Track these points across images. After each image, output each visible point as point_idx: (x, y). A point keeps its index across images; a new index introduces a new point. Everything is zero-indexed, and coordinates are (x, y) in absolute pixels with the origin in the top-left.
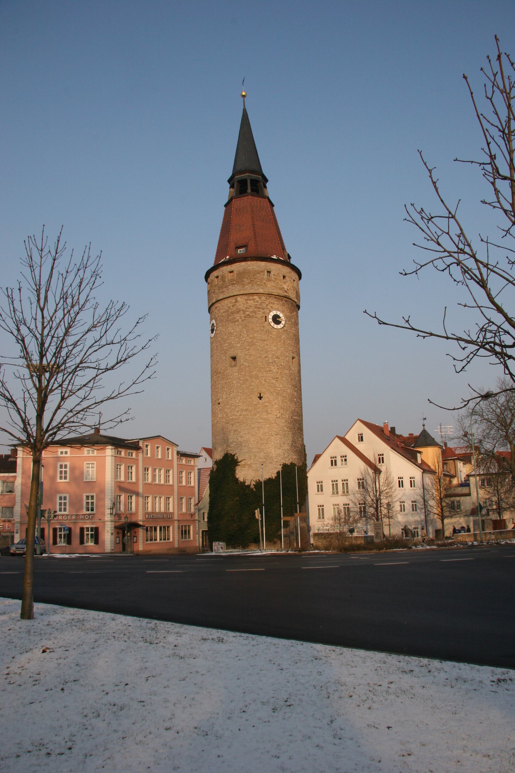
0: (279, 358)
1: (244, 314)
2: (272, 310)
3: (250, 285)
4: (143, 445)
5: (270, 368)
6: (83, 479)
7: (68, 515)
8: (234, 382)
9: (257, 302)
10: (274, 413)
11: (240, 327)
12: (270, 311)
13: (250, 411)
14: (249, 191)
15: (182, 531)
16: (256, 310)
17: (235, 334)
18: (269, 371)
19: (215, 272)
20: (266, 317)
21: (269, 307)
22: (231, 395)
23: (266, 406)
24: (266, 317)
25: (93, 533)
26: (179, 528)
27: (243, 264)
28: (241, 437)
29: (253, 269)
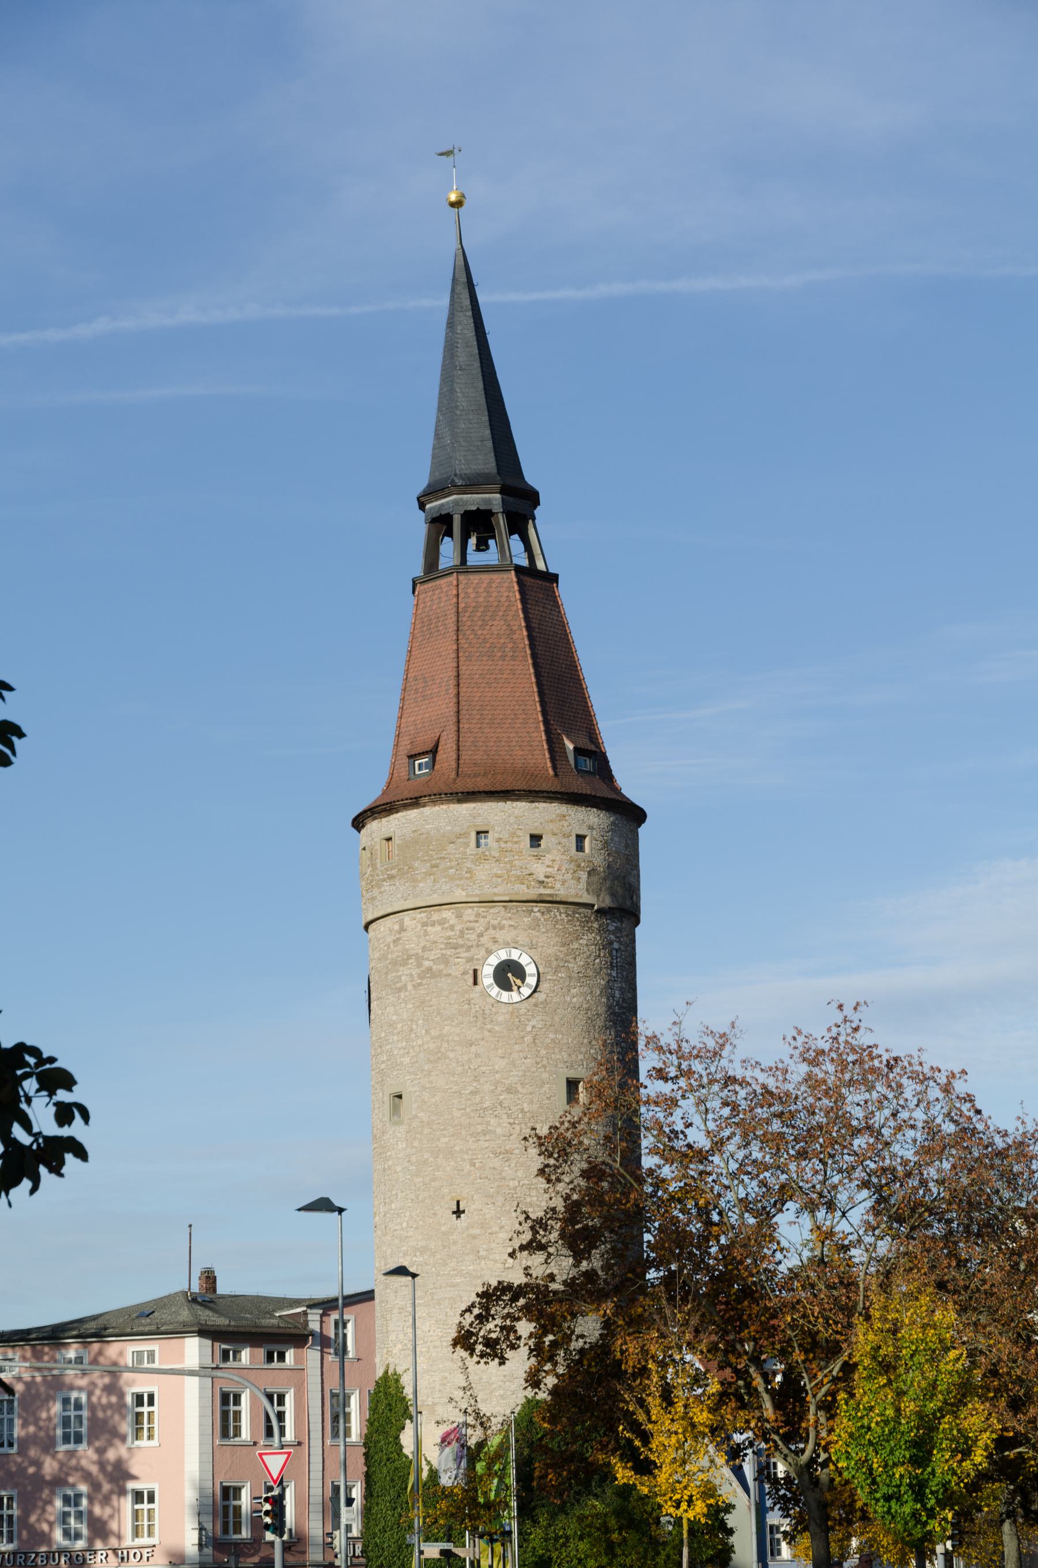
0: (517, 1092)
2: (494, 948)
5: (488, 1123)
11: (410, 1006)
12: (489, 952)
16: (449, 952)
18: (485, 1133)
20: (475, 971)
21: (484, 940)
22: (393, 1206)
23: (475, 1237)
24: (475, 971)
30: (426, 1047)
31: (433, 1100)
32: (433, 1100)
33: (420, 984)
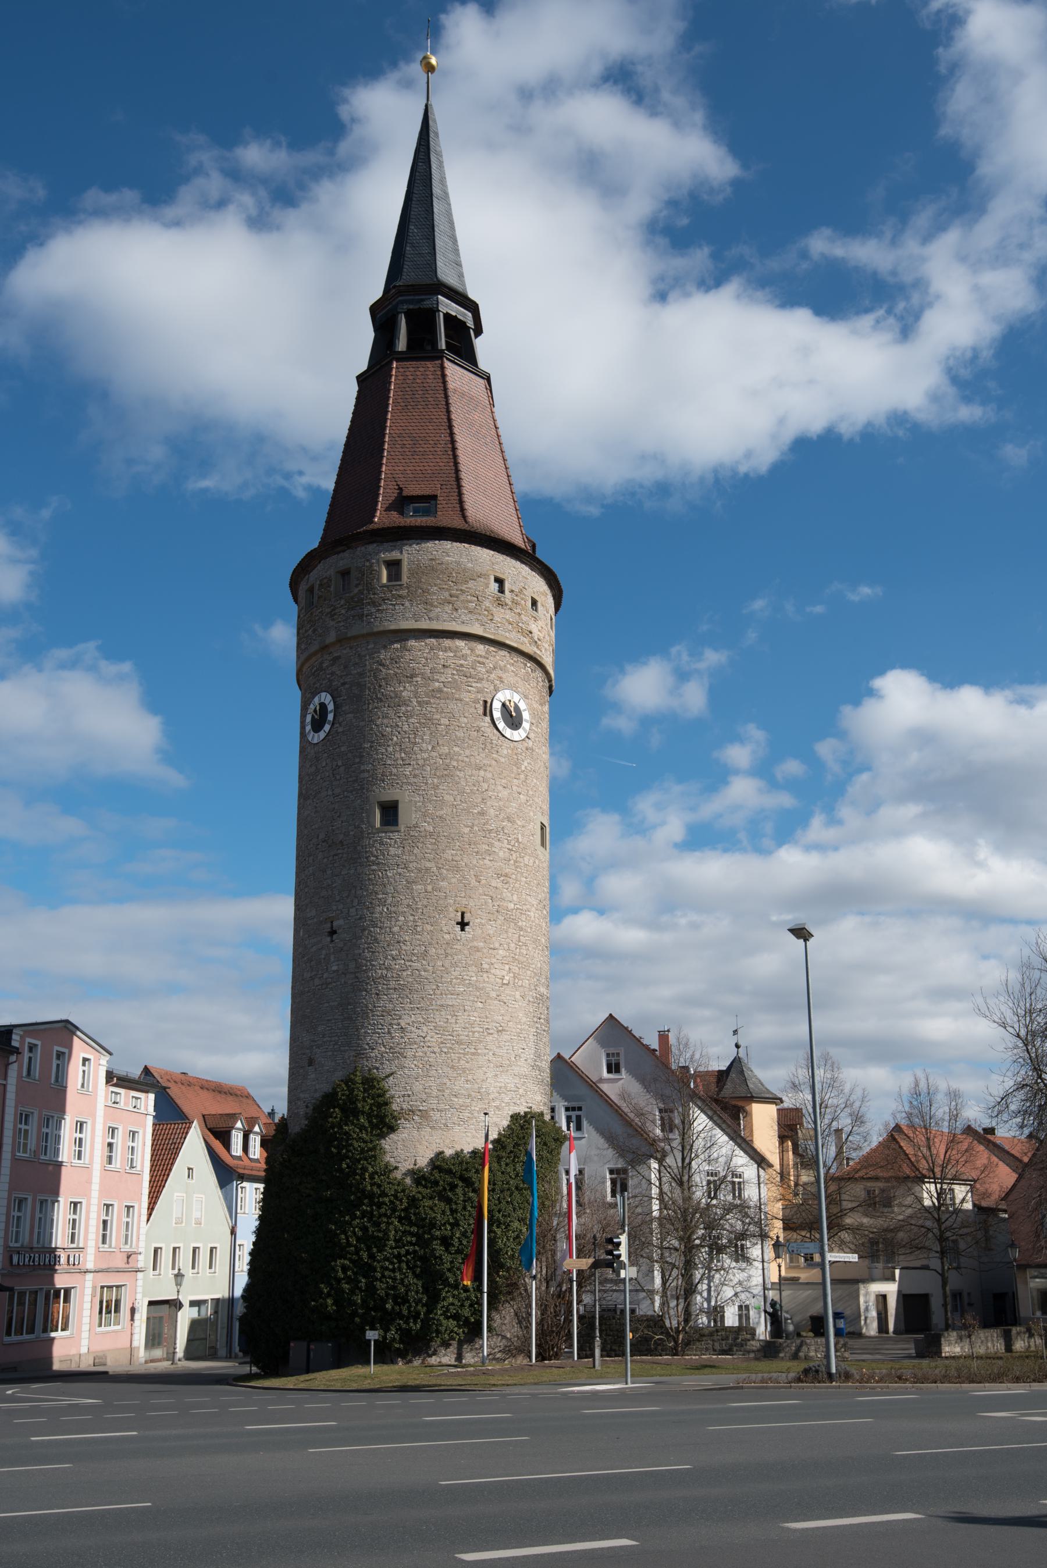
4: (22, 1041)
10: (498, 972)
15: (101, 1302)
19: (527, 569)
21: (493, 676)
26: (93, 1296)
29: (458, 563)
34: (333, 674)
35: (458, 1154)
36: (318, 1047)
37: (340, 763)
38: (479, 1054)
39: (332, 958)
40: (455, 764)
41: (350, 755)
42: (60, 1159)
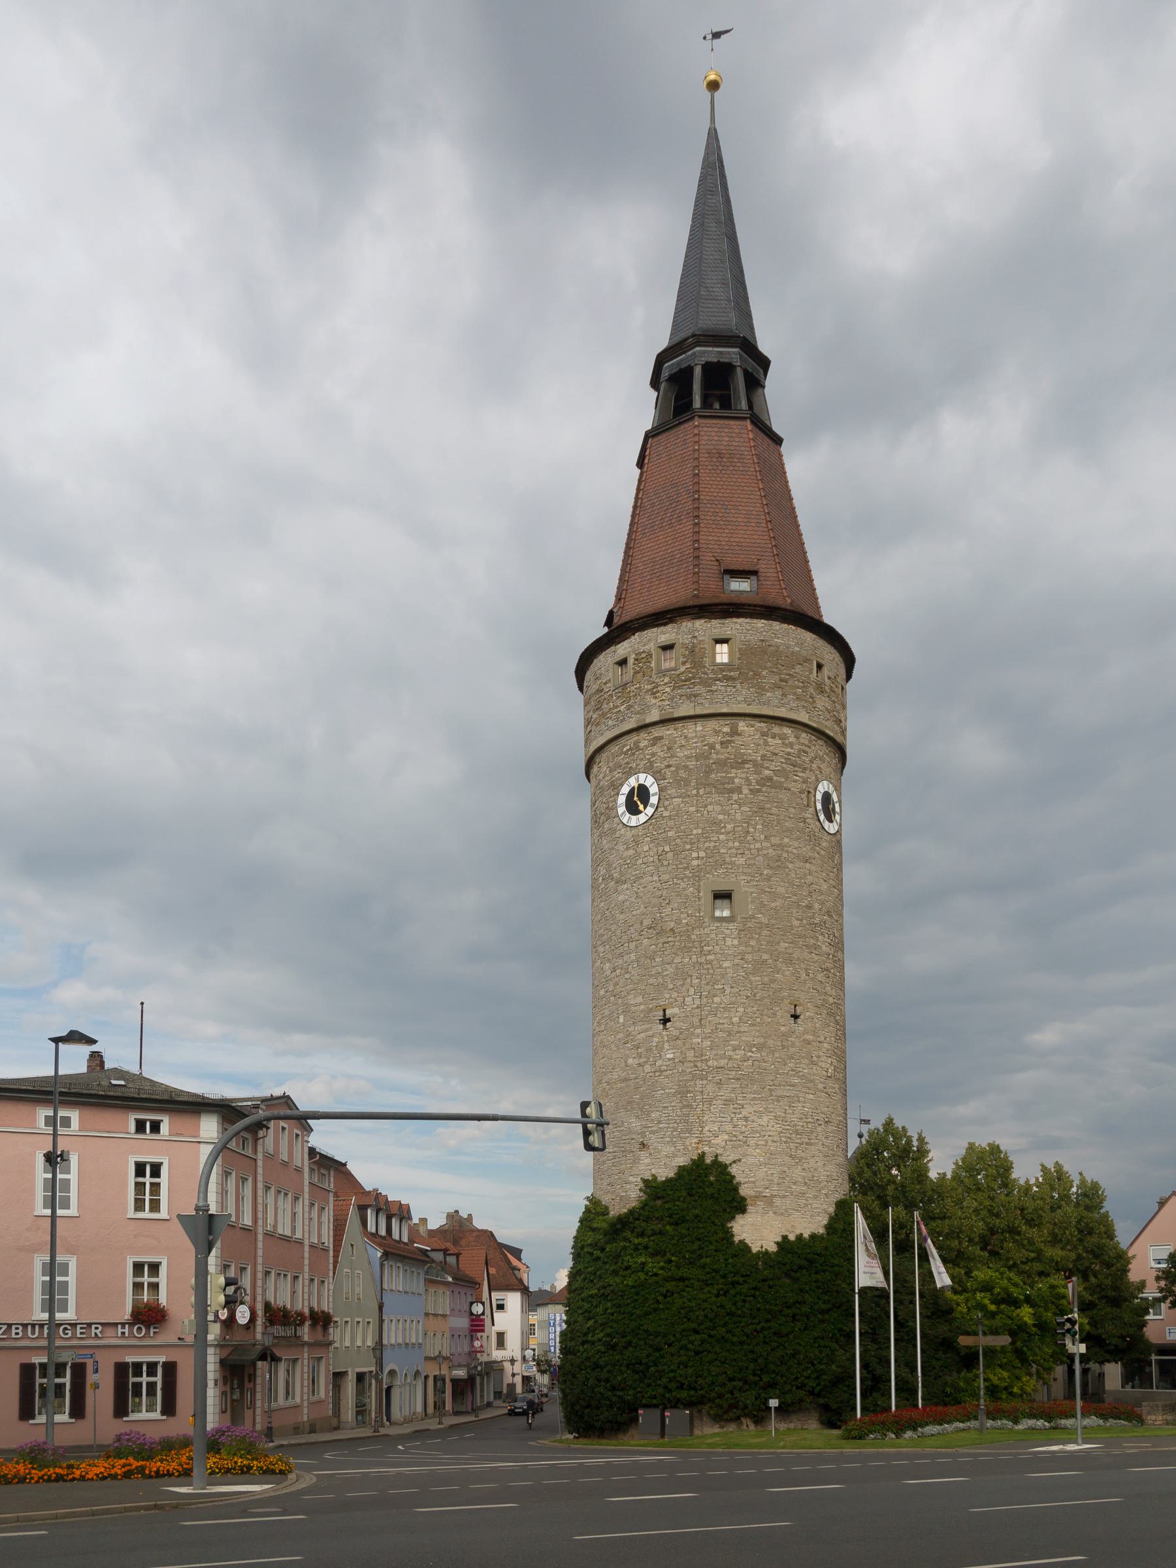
1: (757, 772)
3: (778, 693)
6: (34, 1210)
7: (74, 1325)
8: (726, 964)
9: (791, 745)
13: (773, 1052)
14: (698, 371)
16: (789, 768)
17: (729, 827)
21: (814, 766)
22: (716, 999)
25: (132, 1380)
27: (760, 624)
28: (746, 1119)
30: (765, 852)
31: (773, 905)
32: (773, 905)
33: (759, 791)
34: (653, 755)
35: (800, 1237)
36: (653, 1132)
37: (667, 849)
38: (811, 1144)
39: (666, 1046)
40: (785, 855)
41: (678, 841)
42: (773, 1248)
